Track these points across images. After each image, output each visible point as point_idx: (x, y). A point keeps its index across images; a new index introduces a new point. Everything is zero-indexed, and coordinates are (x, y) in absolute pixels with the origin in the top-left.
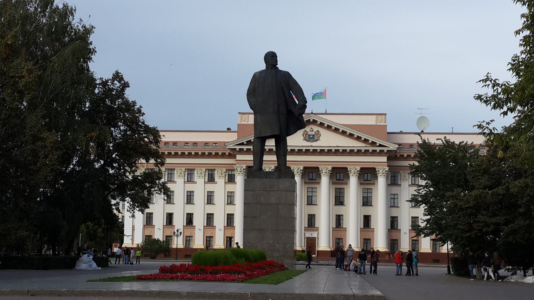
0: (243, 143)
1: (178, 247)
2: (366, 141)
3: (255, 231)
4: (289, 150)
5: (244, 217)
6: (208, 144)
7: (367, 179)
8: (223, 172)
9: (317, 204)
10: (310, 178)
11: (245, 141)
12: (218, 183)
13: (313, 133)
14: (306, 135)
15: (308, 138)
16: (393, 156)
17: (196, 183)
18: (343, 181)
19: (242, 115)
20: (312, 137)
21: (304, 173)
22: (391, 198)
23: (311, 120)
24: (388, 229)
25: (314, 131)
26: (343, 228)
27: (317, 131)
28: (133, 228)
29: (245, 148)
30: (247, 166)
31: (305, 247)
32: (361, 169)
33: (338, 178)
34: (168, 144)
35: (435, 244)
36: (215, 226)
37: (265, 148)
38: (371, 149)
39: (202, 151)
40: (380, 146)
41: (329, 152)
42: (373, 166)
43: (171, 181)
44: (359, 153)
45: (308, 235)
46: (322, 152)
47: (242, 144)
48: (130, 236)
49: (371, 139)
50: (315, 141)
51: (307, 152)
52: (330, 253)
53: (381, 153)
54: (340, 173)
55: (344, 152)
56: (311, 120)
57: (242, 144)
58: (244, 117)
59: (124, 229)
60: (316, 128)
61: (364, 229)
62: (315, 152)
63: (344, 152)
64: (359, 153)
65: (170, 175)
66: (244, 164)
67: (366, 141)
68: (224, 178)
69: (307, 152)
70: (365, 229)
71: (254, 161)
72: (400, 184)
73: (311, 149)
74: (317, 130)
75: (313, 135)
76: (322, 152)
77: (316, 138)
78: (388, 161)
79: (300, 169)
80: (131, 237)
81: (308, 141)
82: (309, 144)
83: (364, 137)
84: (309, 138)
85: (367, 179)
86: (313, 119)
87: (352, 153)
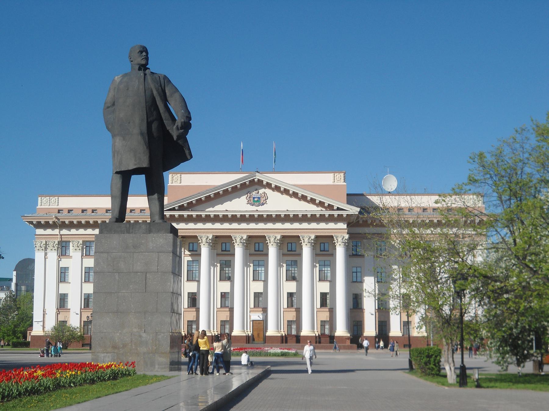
0: (174, 208)
2: (321, 204)
3: (110, 314)
7: (258, 250)
8: (42, 244)
11: (176, 206)
15: (252, 202)
16: (354, 222)
17: (71, 257)
18: (295, 252)
19: (173, 175)
20: (258, 200)
21: (282, 244)
22: (353, 272)
23: (256, 180)
24: (351, 309)
28: (43, 312)
30: (213, 236)
31: (250, 332)
32: (317, 237)
34: (134, 211)
35: (323, 325)
36: (70, 309)
37: (165, 214)
38: (327, 213)
39: (85, 219)
40: (338, 209)
41: (278, 219)
43: (89, 255)
44: (313, 218)
46: (270, 219)
47: (173, 209)
48: (41, 321)
49: (327, 202)
50: (261, 205)
51: (251, 219)
53: (340, 219)
54: (324, 242)
55: (296, 218)
58: (175, 177)
59: (33, 314)
61: (187, 309)
62: (261, 219)
63: (296, 218)
64: (313, 218)
65: (88, 248)
66: (211, 234)
67: (321, 204)
68: (80, 251)
69: (251, 219)
70: (322, 309)
75: (259, 198)
76: (270, 219)
79: (345, 238)
80: (42, 323)
81: (253, 205)
82: (254, 208)
83: (318, 199)
85: (258, 250)
86: (258, 179)
87: (304, 218)
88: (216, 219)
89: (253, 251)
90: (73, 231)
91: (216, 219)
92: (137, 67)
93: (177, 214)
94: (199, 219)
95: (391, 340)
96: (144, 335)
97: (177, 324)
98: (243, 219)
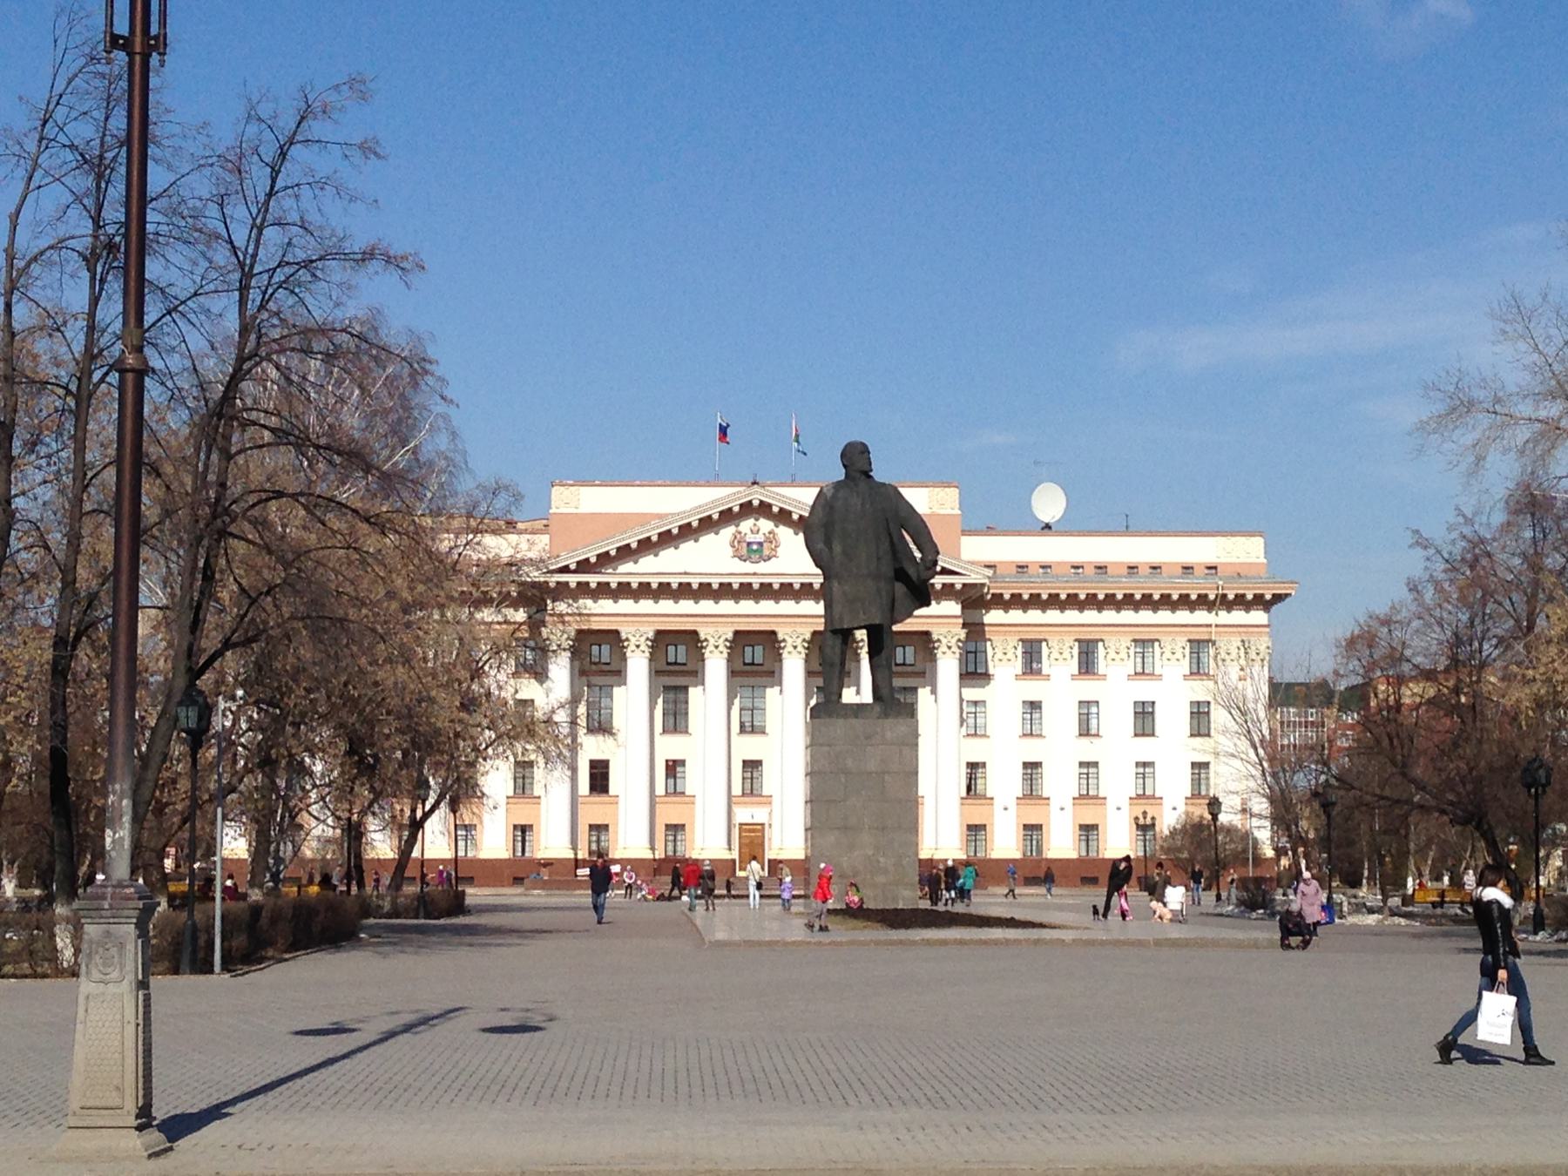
1: (426, 857)
4: (938, 587)
5: (917, 773)
6: (1081, 570)
9: (988, 734)
10: (747, 661)
12: (1164, 678)
13: (760, 538)
14: (739, 542)
23: (756, 503)
24: (1074, 799)
25: (761, 532)
26: (761, 796)
27: (770, 533)
29: (573, 580)
32: (737, 633)
33: (671, 659)
42: (924, 628)
45: (743, 815)
47: (565, 570)
50: (765, 561)
51: (745, 591)
52: (1110, 866)
56: (756, 503)
57: (565, 570)
60: (765, 525)
62: (767, 592)
69: (745, 591)
71: (825, 616)
72: (618, 669)
73: (756, 582)
74: (769, 530)
75: (760, 544)
77: (766, 552)
78: (966, 611)
81: (745, 561)
82: (748, 567)
84: (748, 551)
88: (664, 591)
89: (739, 666)
90: (1224, 617)
91: (664, 591)
92: (415, 278)
93: (573, 580)
94: (624, 591)
95: (126, 847)
96: (881, 860)
97: (754, 831)
98: (724, 591)
